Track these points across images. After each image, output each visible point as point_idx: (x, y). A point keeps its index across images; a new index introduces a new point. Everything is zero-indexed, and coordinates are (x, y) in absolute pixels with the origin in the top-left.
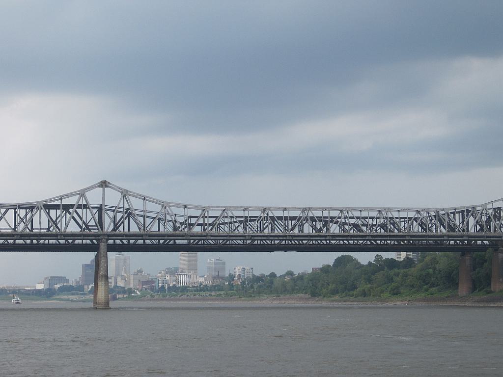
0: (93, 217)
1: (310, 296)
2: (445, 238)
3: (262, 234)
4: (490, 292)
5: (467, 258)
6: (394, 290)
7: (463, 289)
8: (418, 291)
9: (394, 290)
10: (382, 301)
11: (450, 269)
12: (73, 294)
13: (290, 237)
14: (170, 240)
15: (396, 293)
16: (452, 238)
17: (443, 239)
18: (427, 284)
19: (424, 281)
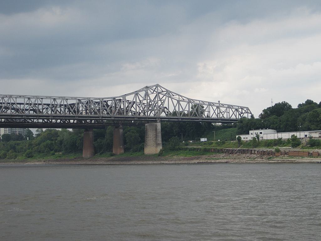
0: (233, 113)
1: (123, 151)
2: (100, 118)
3: (6, 114)
4: (112, 155)
5: (91, 133)
6: (29, 154)
7: (87, 153)
8: (46, 155)
9: (29, 154)
10: (313, 149)
11: (74, 140)
12: (194, 146)
13: (52, 117)
14: (66, 120)
15: (30, 156)
16: (58, 118)
17: (98, 119)
18: (52, 150)
19: (50, 148)
